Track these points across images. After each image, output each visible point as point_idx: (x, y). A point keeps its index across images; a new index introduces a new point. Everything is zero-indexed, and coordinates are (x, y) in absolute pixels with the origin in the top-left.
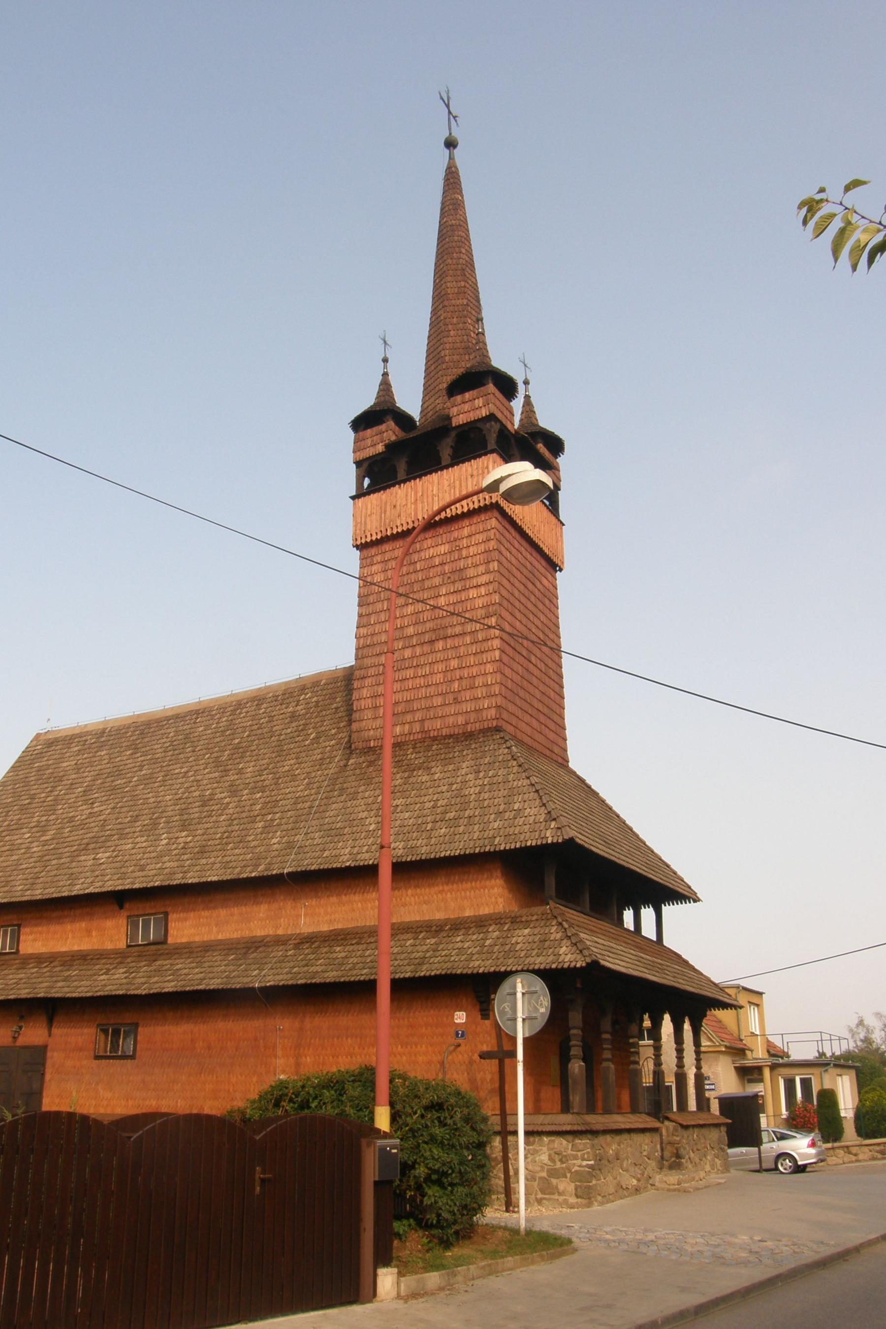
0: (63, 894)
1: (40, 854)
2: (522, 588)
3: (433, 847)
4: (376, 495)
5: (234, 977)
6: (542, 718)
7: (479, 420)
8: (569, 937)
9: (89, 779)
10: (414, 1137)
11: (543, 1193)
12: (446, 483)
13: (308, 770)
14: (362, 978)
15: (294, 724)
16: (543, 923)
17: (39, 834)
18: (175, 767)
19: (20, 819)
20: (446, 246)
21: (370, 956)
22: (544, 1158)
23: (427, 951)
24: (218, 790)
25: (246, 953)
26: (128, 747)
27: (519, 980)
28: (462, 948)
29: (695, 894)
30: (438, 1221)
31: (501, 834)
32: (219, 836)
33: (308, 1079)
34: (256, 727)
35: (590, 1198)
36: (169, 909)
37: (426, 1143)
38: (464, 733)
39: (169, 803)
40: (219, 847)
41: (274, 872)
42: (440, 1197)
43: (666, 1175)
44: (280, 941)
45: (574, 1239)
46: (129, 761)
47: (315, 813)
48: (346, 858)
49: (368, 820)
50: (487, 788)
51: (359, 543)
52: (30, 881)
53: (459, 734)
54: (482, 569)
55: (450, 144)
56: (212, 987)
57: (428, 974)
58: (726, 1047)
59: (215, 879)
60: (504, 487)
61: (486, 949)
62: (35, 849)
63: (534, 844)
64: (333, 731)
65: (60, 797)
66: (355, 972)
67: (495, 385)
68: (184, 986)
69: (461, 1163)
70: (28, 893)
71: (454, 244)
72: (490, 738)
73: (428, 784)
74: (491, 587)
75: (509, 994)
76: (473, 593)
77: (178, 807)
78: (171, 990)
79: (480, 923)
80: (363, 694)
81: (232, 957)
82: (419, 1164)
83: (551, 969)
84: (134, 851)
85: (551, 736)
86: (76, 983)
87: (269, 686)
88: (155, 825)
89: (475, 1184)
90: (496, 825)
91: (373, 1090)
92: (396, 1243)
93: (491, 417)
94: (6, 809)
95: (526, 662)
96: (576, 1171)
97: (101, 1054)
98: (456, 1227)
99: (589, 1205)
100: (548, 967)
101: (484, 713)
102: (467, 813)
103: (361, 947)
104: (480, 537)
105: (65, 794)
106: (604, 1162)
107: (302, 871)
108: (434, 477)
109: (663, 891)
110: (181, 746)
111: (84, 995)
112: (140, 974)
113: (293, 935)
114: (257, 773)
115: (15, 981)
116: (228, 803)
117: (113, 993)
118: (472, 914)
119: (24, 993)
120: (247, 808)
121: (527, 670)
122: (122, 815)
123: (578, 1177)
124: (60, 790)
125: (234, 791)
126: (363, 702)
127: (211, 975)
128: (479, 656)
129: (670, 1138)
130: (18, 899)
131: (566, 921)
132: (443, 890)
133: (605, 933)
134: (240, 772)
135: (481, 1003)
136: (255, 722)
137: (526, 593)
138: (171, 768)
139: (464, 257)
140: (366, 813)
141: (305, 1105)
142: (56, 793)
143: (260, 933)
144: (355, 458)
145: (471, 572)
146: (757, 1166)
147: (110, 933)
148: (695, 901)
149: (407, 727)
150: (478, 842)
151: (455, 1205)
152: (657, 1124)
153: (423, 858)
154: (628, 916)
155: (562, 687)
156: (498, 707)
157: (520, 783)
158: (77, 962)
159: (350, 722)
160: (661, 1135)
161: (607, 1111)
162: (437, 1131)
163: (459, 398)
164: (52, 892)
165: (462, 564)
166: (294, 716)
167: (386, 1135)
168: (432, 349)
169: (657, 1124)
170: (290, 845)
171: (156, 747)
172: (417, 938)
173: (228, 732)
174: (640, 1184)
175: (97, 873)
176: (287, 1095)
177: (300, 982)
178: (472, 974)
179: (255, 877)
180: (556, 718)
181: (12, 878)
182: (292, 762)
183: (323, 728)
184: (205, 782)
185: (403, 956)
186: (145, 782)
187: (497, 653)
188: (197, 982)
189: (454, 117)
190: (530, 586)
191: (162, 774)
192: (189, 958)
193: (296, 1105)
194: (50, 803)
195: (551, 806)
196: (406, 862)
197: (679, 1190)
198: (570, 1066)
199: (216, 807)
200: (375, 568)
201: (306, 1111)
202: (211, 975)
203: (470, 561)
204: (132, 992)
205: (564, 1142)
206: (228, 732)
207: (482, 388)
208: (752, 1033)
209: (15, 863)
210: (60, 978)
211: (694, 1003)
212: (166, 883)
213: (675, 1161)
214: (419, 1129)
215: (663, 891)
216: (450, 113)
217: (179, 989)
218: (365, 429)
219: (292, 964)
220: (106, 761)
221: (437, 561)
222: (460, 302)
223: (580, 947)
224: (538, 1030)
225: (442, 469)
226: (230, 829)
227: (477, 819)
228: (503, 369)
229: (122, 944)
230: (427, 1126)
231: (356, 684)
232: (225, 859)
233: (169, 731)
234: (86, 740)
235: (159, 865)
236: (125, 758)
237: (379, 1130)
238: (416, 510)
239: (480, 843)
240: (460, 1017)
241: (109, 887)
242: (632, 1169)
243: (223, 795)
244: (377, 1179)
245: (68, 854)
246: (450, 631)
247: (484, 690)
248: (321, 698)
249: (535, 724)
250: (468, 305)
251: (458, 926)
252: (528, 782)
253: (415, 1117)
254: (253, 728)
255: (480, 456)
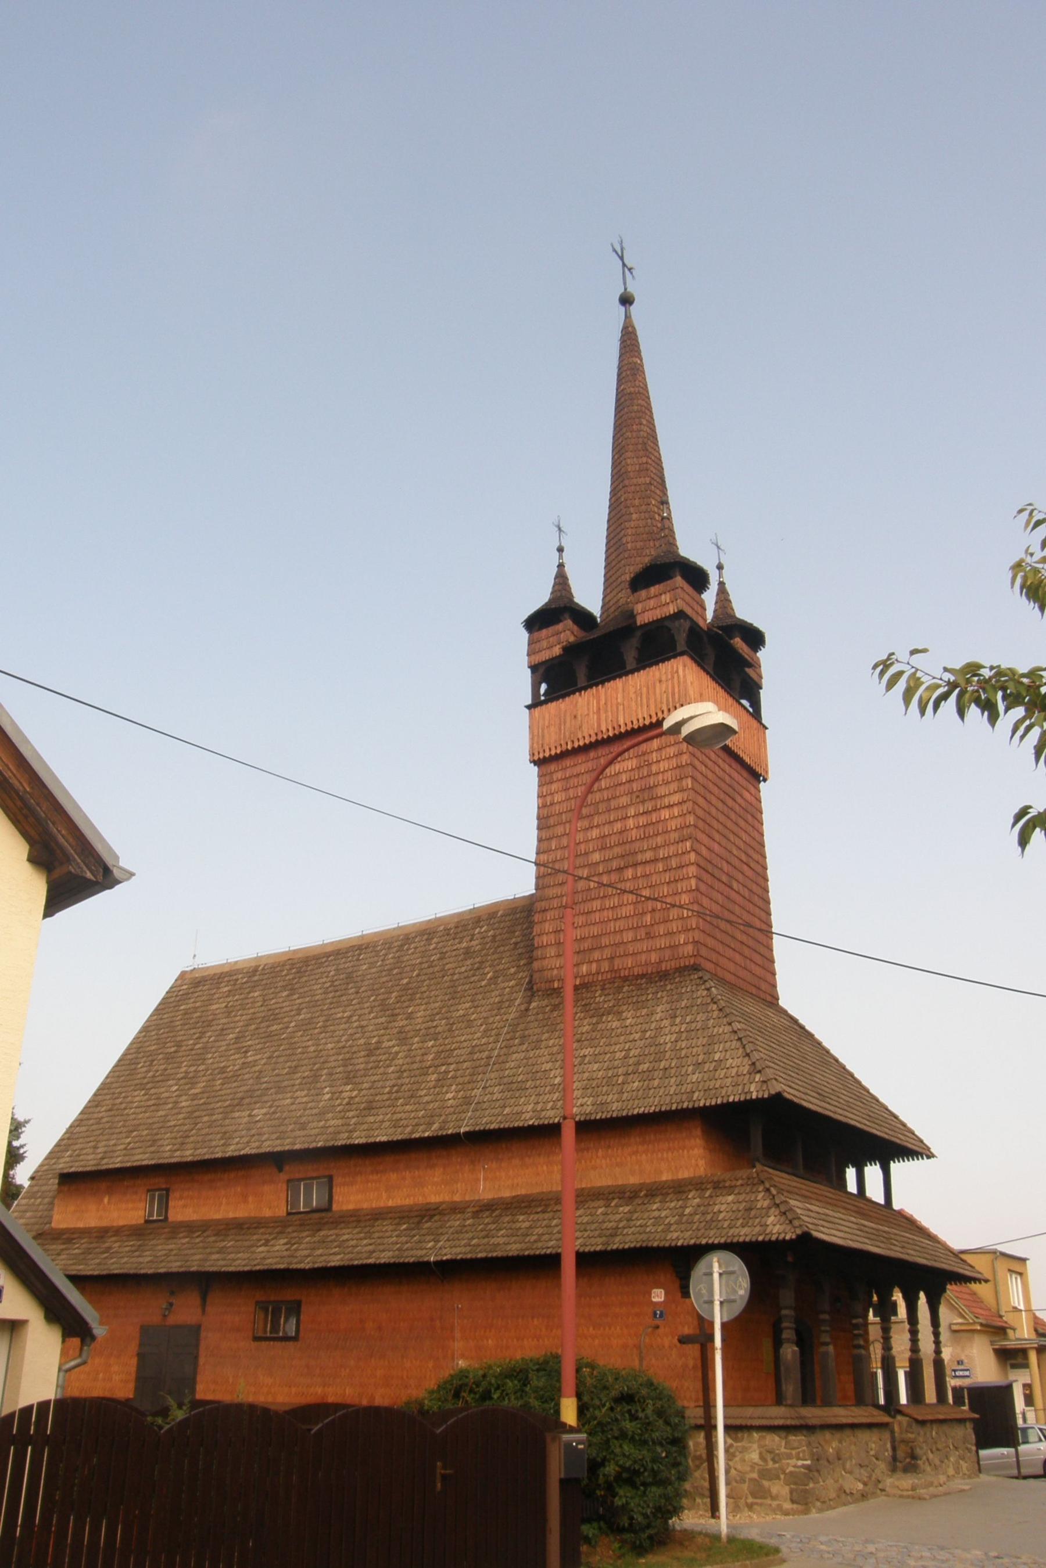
0: (217, 1156)
1: (189, 1109)
2: (720, 805)
3: (625, 1103)
4: (554, 704)
5: (407, 1249)
6: (747, 952)
7: (666, 618)
8: (778, 1206)
9: (241, 1024)
10: (603, 1432)
11: (754, 1496)
12: (632, 690)
13: (484, 1015)
14: (548, 1252)
15: (469, 962)
16: (748, 1189)
17: (187, 1087)
18: (337, 1010)
19: (166, 1070)
20: (626, 417)
21: (556, 1226)
22: (755, 1456)
23: (620, 1220)
24: (386, 1038)
25: (419, 1223)
26: (284, 988)
27: (715, 1259)
28: (659, 1217)
29: (929, 1149)
30: (631, 1525)
31: (700, 1087)
32: (387, 1090)
33: (490, 1367)
34: (426, 965)
35: (806, 1504)
36: (334, 1172)
37: (617, 1438)
38: (658, 972)
39: (331, 1053)
40: (388, 1103)
41: (450, 1132)
42: (632, 1498)
43: (898, 1479)
44: (456, 1209)
45: (784, 1549)
46: (284, 1004)
47: (494, 1064)
48: (528, 1116)
49: (553, 1072)
50: (684, 1035)
51: (536, 758)
52: (179, 1140)
53: (652, 973)
54: (674, 786)
55: (626, 300)
56: (383, 1261)
57: (621, 1247)
58: (981, 1325)
59: (384, 1139)
60: (686, 731)
61: (685, 1218)
62: (183, 1104)
63: (736, 1100)
64: (513, 970)
65: (210, 1045)
66: (540, 1245)
67: (684, 577)
68: (351, 1259)
69: (654, 1461)
70: (178, 1153)
71: (633, 415)
72: (687, 978)
73: (619, 1031)
74: (685, 807)
75: (706, 1274)
76: (665, 814)
77: (341, 1057)
78: (337, 1264)
79: (679, 1188)
80: (545, 931)
81: (405, 1226)
82: (609, 1461)
83: (757, 1241)
84: (294, 1107)
85: (758, 971)
86: (233, 1255)
87: (440, 918)
88: (316, 1077)
89: (670, 1484)
90: (694, 1078)
91: (559, 1381)
92: (584, 1548)
93: (680, 615)
94: (150, 1058)
95: (728, 889)
96: (791, 1472)
97: (260, 1334)
98: (651, 1531)
99: (806, 1512)
100: (754, 1239)
101: (680, 950)
102: (662, 1064)
103: (546, 1216)
104: (672, 751)
105: (215, 1041)
106: (824, 1462)
107: (480, 1131)
108: (618, 683)
109: (892, 1146)
110: (343, 987)
111: (241, 1269)
112: (302, 1246)
113: (472, 1201)
114: (428, 1018)
115: (164, 1252)
116: (397, 1053)
117: (274, 1267)
118: (670, 1178)
119: (175, 1266)
120: (418, 1059)
121: (728, 898)
122: (280, 1066)
123: (793, 1479)
124: (210, 1036)
125: (403, 1038)
126: (545, 938)
127: (381, 1247)
128: (673, 885)
129: (904, 1436)
130: (166, 1161)
131: (775, 1186)
132: (637, 1152)
133: (821, 1198)
134: (410, 1017)
135: (681, 1279)
136: (425, 959)
137: (725, 809)
138: (333, 1011)
139: (645, 428)
140: (550, 1064)
141: (486, 1396)
142: (205, 1040)
143: (434, 1199)
144: (529, 662)
145: (662, 791)
146: (1015, 1472)
147: (269, 1200)
148: (928, 1157)
149: (594, 965)
150: (675, 1097)
151: (648, 1506)
152: (886, 1419)
153: (614, 1115)
154: (851, 1173)
155: (770, 914)
156: (696, 942)
157: (721, 1030)
158: (233, 1231)
159: (531, 960)
160: (892, 1432)
161: (827, 1403)
162: (628, 1425)
163: (643, 593)
164: (203, 1153)
165: (652, 781)
166: (468, 953)
167: (572, 1430)
168: (612, 535)
169: (886, 1419)
170: (467, 1101)
171: (315, 987)
172: (609, 1206)
173: (395, 972)
174: (867, 1489)
175: (253, 1132)
176: (466, 1385)
177: (480, 1255)
178: (670, 1247)
179: (428, 1137)
180: (762, 950)
181: (159, 1137)
182: (468, 1005)
183: (501, 967)
184: (371, 1028)
185: (593, 1226)
186: (304, 1028)
187: (693, 882)
188: (365, 1255)
189: (630, 270)
190: (730, 802)
191: (323, 1018)
192: (356, 1227)
193: (477, 1396)
194: (199, 1051)
195: (756, 1056)
196: (595, 1120)
197: (913, 1498)
198: (781, 1351)
199: (384, 1057)
200: (554, 787)
201: (487, 1403)
202: (381, 1247)
203: (660, 777)
204: (294, 1266)
205: (777, 1438)
206: (395, 972)
207: (669, 582)
208: (1015, 1308)
209: (162, 1119)
210: (214, 1250)
211: (931, 1276)
212: (331, 1144)
213: (909, 1463)
214: (609, 1423)
215: (892, 1146)
216: (624, 265)
217: (346, 1263)
218: (540, 629)
219: (470, 1235)
220: (260, 1004)
221: (624, 778)
222: (641, 480)
223: (790, 1217)
224: (737, 1314)
225: (627, 674)
226: (400, 1082)
227: (673, 1071)
228: (692, 559)
229: (281, 1211)
230: (617, 1420)
231: (536, 918)
232: (395, 1117)
233: (329, 969)
234: (237, 980)
235: (322, 1124)
236: (281, 1000)
237: (565, 1424)
238: (599, 719)
239: (678, 1098)
240: (658, 1296)
241: (267, 1147)
242: (857, 1470)
243: (391, 1043)
244: (562, 1476)
245: (221, 1110)
246: (640, 857)
247: (680, 923)
248: (498, 932)
249: (738, 958)
250: (650, 484)
251: (654, 1191)
252: (728, 1029)
253: (604, 1410)
254: (423, 966)
255: (668, 659)
